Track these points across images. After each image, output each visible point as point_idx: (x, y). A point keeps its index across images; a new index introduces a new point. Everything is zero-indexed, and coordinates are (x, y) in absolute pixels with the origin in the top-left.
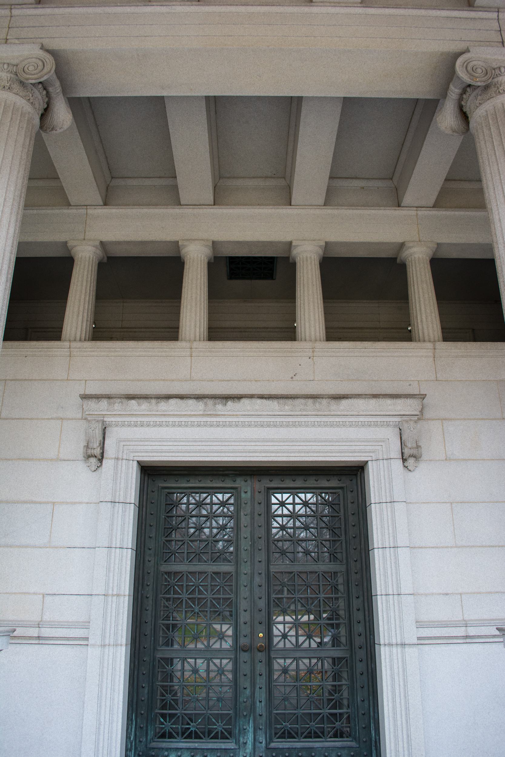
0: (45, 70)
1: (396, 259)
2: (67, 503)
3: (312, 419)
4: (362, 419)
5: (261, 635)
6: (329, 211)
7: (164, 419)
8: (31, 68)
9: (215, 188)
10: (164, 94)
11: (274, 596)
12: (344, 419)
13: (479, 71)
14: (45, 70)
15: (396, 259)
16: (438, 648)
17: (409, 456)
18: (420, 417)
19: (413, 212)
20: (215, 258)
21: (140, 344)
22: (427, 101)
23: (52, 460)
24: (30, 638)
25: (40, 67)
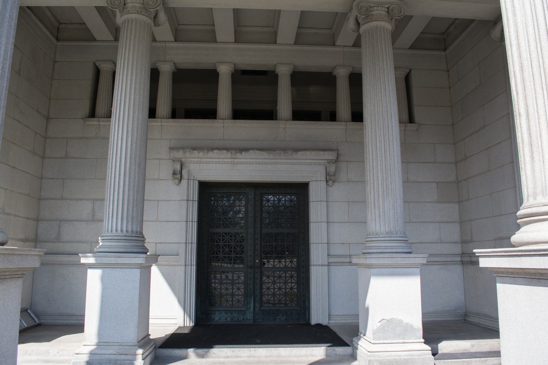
0: (158, 4)
2: (165, 201)
3: (284, 161)
4: (307, 161)
6: (296, 47)
7: (211, 160)
8: (151, 2)
9: (235, 31)
10: (213, 7)
12: (299, 161)
13: (364, 9)
14: (158, 4)
16: (338, 267)
17: (330, 179)
18: (337, 161)
20: (235, 70)
21: (197, 120)
22: (342, 13)
23: (156, 180)
24: (346, 263)
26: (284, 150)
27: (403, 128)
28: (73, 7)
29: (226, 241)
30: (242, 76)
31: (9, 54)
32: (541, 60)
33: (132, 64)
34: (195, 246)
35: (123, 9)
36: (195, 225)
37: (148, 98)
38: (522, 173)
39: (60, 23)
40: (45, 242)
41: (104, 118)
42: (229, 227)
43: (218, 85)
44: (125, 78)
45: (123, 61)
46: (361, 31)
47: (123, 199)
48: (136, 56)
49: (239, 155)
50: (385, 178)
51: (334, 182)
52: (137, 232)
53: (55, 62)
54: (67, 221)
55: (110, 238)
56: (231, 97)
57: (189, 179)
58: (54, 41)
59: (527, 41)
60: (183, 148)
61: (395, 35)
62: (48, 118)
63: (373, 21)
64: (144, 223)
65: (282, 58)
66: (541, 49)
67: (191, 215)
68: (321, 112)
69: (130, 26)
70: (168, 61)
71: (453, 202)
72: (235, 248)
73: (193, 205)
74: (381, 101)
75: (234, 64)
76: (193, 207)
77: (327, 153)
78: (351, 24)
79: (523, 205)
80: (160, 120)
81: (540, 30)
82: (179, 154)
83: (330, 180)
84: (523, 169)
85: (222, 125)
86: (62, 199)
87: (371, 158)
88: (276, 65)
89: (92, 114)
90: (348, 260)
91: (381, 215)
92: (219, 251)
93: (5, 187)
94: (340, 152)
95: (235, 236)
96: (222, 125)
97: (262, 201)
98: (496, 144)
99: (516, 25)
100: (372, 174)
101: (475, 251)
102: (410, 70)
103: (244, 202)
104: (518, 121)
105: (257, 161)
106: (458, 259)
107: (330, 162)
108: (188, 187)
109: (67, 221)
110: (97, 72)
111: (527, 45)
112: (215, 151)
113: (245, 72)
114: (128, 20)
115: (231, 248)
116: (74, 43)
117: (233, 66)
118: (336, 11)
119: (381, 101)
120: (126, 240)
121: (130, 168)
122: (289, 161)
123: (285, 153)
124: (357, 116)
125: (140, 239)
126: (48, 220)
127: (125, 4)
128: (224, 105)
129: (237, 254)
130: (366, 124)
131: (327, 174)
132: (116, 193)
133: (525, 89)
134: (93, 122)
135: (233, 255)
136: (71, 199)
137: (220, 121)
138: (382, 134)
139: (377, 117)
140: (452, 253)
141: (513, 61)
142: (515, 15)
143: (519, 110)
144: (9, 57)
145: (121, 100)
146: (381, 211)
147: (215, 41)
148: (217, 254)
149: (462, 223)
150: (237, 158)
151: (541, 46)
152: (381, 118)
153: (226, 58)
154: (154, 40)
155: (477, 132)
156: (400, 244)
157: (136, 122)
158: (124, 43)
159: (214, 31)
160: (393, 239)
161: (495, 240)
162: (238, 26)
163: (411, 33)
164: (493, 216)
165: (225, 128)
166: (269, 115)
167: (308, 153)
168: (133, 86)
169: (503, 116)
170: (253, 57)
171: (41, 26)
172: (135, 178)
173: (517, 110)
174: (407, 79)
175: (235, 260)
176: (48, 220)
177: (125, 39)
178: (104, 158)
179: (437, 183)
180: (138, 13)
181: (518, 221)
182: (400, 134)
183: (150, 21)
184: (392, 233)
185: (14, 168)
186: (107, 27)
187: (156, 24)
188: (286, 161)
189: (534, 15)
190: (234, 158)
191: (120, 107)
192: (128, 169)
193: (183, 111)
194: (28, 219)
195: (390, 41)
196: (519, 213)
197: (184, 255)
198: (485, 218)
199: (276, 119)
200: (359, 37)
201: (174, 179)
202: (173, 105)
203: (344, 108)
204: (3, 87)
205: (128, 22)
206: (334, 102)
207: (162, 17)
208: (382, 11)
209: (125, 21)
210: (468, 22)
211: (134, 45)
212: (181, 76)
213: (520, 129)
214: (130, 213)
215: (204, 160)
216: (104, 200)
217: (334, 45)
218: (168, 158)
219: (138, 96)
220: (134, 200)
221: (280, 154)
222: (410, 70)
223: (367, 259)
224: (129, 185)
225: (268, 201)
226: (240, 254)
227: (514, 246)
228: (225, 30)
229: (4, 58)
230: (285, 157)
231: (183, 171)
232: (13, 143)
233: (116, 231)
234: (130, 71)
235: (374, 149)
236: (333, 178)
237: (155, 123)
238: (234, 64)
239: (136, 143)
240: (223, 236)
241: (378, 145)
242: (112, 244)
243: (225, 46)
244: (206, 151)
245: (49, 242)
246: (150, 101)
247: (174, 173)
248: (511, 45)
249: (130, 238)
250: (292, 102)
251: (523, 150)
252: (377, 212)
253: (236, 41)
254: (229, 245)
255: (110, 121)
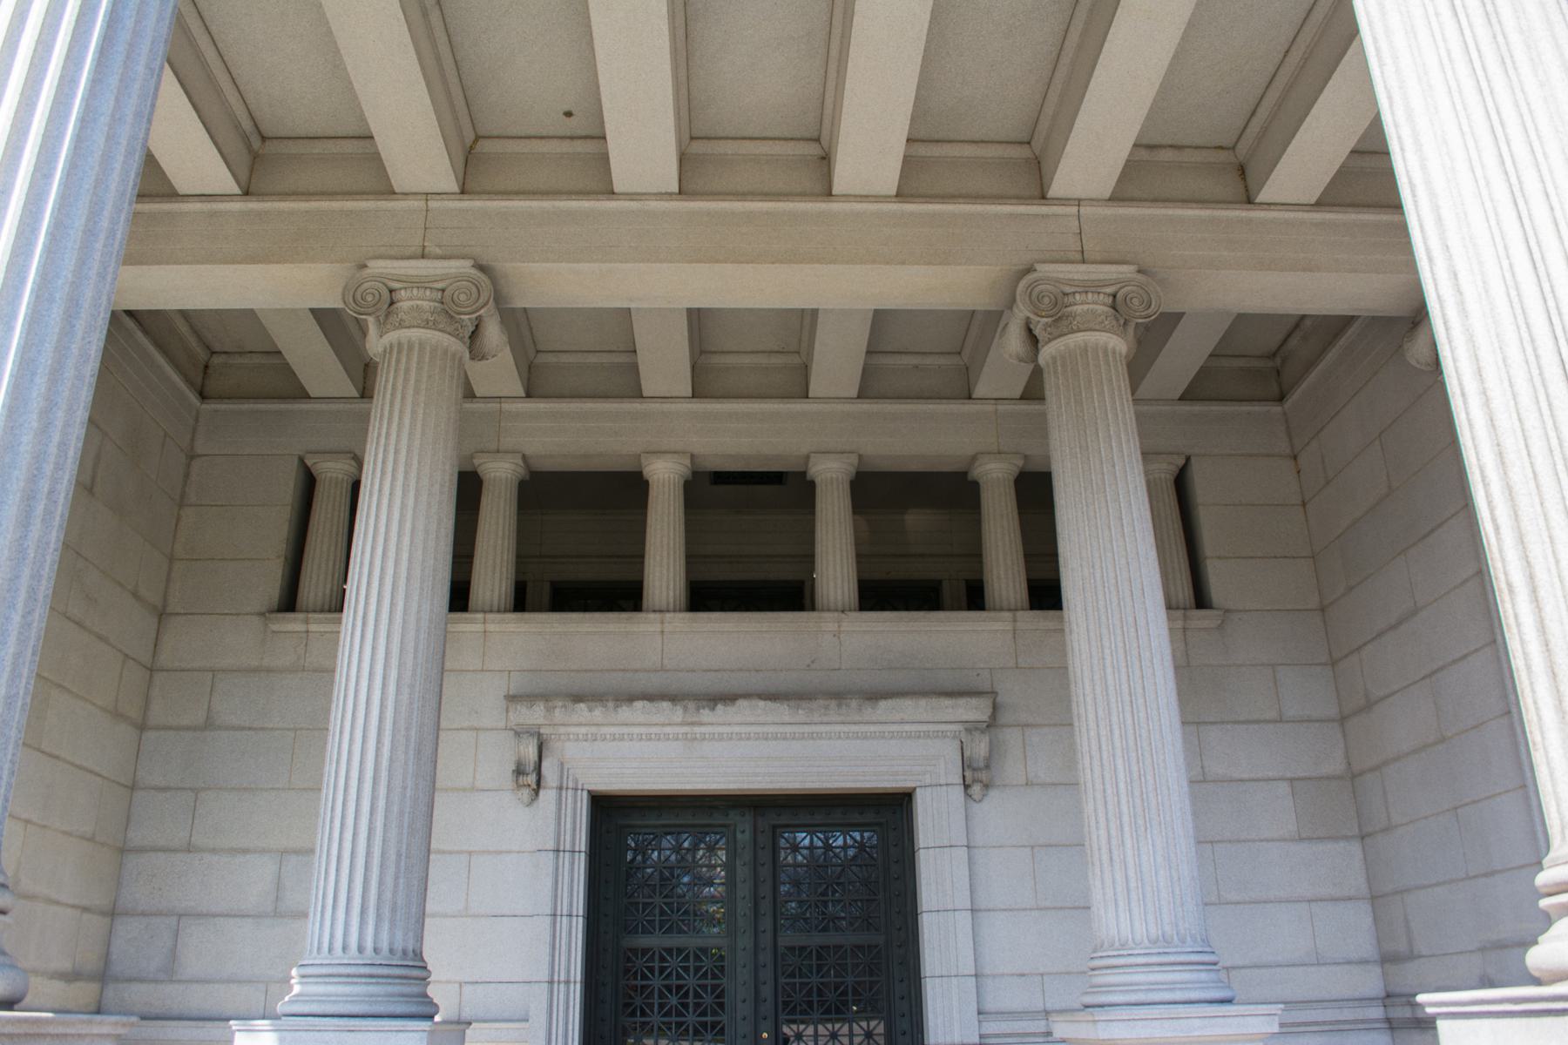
1: (965, 474)
2: (489, 852)
3: (838, 728)
4: (907, 728)
5: (765, 1035)
7: (625, 730)
8: (463, 297)
9: (693, 368)
10: (632, 305)
11: (782, 980)
13: (1046, 300)
15: (965, 474)
17: (976, 777)
18: (992, 724)
19: (989, 408)
21: (588, 615)
22: (988, 313)
23: (464, 790)
25: (475, 295)
26: (839, 696)
27: (1179, 624)
28: (252, 310)
29: (670, 974)
30: (713, 489)
31: (71, 453)
32: (1552, 434)
33: (408, 465)
34: (577, 991)
35: (387, 315)
36: (579, 925)
37: (449, 558)
38: (1538, 757)
39: (213, 353)
40: (130, 980)
41: (322, 611)
42: (680, 931)
43: (645, 515)
44: (385, 501)
45: (380, 456)
46: (1041, 360)
47: (368, 854)
48: (417, 443)
49: (706, 715)
50: (1135, 775)
51: (987, 786)
52: (405, 952)
53: (192, 457)
54: (200, 915)
55: (324, 971)
56: (683, 549)
57: (560, 788)
58: (193, 398)
59: (1506, 384)
60: (546, 697)
61: (1137, 368)
62: (162, 615)
63: (1073, 332)
64: (427, 920)
65: (826, 435)
66: (1550, 405)
67: (566, 895)
68: (940, 582)
69: (404, 360)
70: (506, 452)
71: (1346, 838)
72: (697, 995)
73: (572, 864)
74: (1111, 546)
75: (692, 456)
76: (572, 870)
77: (962, 701)
78: (1013, 341)
79: (1551, 855)
80: (480, 616)
81: (1541, 352)
82: (534, 715)
83: (974, 781)
84: (1540, 746)
85: (658, 627)
86: (189, 848)
87: (1091, 716)
88: (808, 457)
89: (289, 602)
90: (1040, 1026)
91: (1133, 885)
92: (651, 1006)
93: (25, 816)
94: (999, 699)
95: (697, 958)
96: (658, 627)
97: (775, 850)
98: (1455, 662)
99: (1471, 339)
100: (1096, 763)
101: (1421, 998)
102: (1188, 459)
103: (722, 855)
104: (1508, 606)
105: (759, 729)
106: (1376, 1012)
107: (972, 728)
108: (559, 810)
109: (200, 915)
110: (309, 484)
111: (1509, 393)
112: (639, 704)
113: (722, 478)
114: (400, 344)
115: (686, 995)
116: (247, 406)
117: (688, 462)
118: (971, 308)
119: (1111, 546)
120: (371, 976)
121: (391, 759)
122: (854, 728)
123: (839, 706)
124: (1045, 593)
125: (415, 973)
126: (143, 914)
127: (392, 303)
128: (664, 571)
129: (703, 1014)
130: (1073, 618)
131: (966, 764)
132: (348, 836)
133: (1516, 513)
134: (292, 624)
135: (691, 1018)
136: (214, 851)
137: (652, 616)
138: (1120, 645)
139: (1101, 597)
140: (1357, 995)
141: (1473, 439)
142: (1464, 312)
143: (1506, 574)
144: (70, 461)
145: (371, 563)
146: (1131, 873)
147: (638, 394)
148: (643, 1014)
149: (1375, 899)
150: (701, 724)
151: (1548, 396)
152: (1115, 600)
153: (669, 438)
154: (470, 394)
155: (1393, 628)
156: (1194, 976)
157: (412, 625)
158: (387, 408)
159: (634, 368)
160: (1172, 959)
161: (1482, 949)
162: (702, 352)
163: (1182, 358)
164: (1469, 878)
165: (667, 637)
166: (791, 595)
167: (908, 703)
168: (408, 525)
169: (1466, 581)
170: (744, 434)
171: (160, 359)
172: (405, 788)
173: (1502, 577)
174: (1181, 484)
175: (696, 1032)
176: (143, 914)
177: (388, 396)
178: (319, 727)
179: (1291, 780)
180: (426, 325)
181: (1544, 903)
182: (1172, 642)
183: (459, 347)
184: (1167, 941)
185: (57, 757)
186: (342, 362)
187: (476, 353)
188: (845, 728)
189: (1519, 311)
190: (693, 724)
191: (369, 583)
192: (385, 763)
193: (549, 590)
194: (85, 909)
195: (1124, 384)
196: (1542, 879)
197: (542, 1019)
198: (1444, 883)
199: (813, 609)
200: (1037, 375)
201: (519, 786)
202: (517, 572)
203: (1004, 571)
204: (48, 543)
205: (399, 352)
206: (975, 554)
207: (493, 333)
208: (1096, 305)
209: (391, 346)
210: (1337, 326)
211: (414, 412)
212: (543, 491)
213: (1515, 630)
214: (388, 895)
215: (605, 730)
216: (311, 851)
217: (970, 398)
218: (502, 724)
219: (420, 552)
220: (399, 855)
221: (827, 708)
222: (1188, 459)
223: (1101, 1025)
224: (387, 810)
225: (795, 848)
226: (714, 1013)
227: (1538, 982)
228: (665, 363)
229: (57, 464)
230: (841, 718)
231: (544, 764)
232: (60, 686)
233: (345, 948)
234: (399, 483)
235: (1098, 689)
236: (983, 776)
237: (468, 625)
238: (692, 456)
239: (412, 686)
240: (663, 959)
241: (1110, 678)
242: (331, 989)
243: (667, 407)
244: (611, 704)
245: (142, 980)
246: (454, 563)
247: (519, 771)
248: (1463, 395)
249: (385, 971)
250: (858, 556)
251: (1533, 691)
252: (1119, 877)
253: (696, 394)
254: (679, 987)
255: (339, 621)
